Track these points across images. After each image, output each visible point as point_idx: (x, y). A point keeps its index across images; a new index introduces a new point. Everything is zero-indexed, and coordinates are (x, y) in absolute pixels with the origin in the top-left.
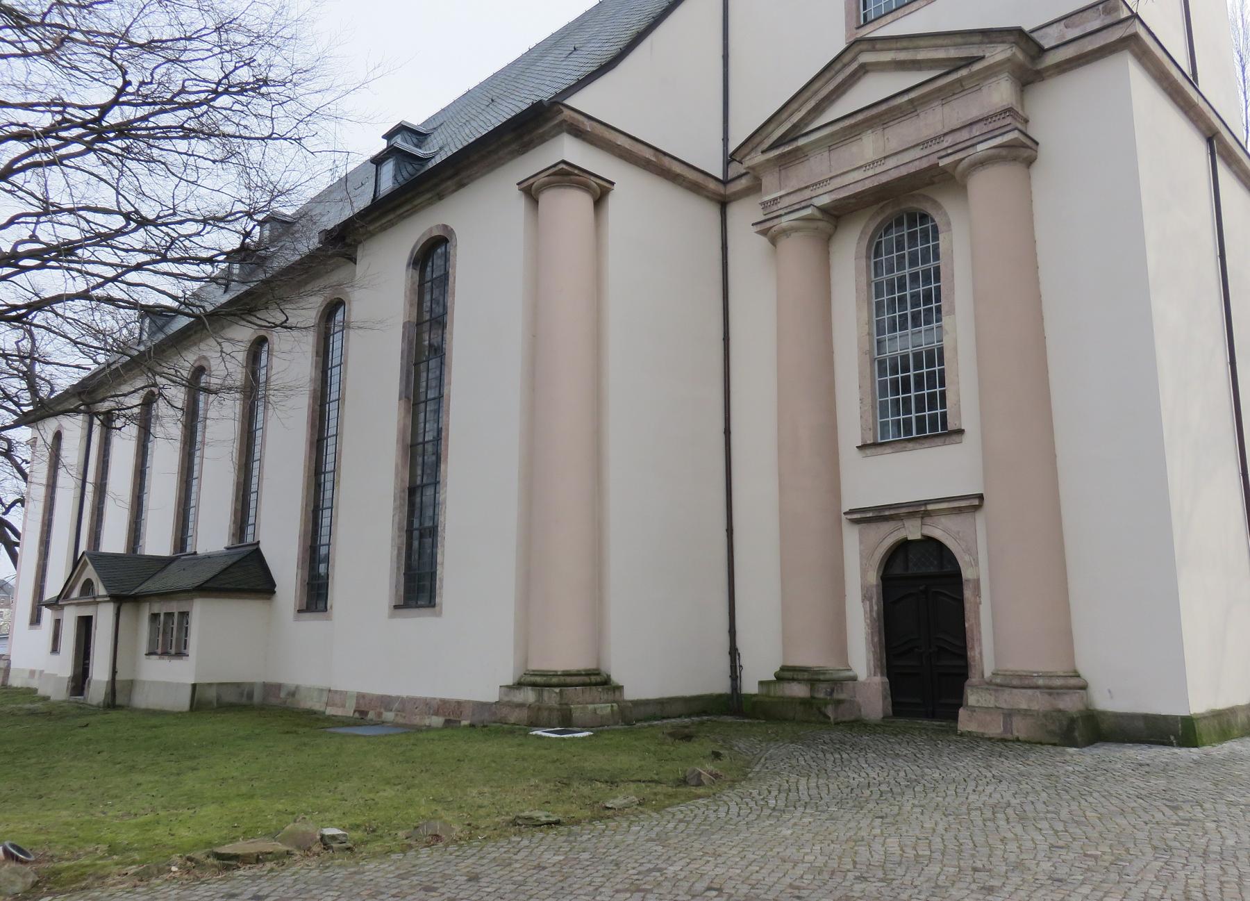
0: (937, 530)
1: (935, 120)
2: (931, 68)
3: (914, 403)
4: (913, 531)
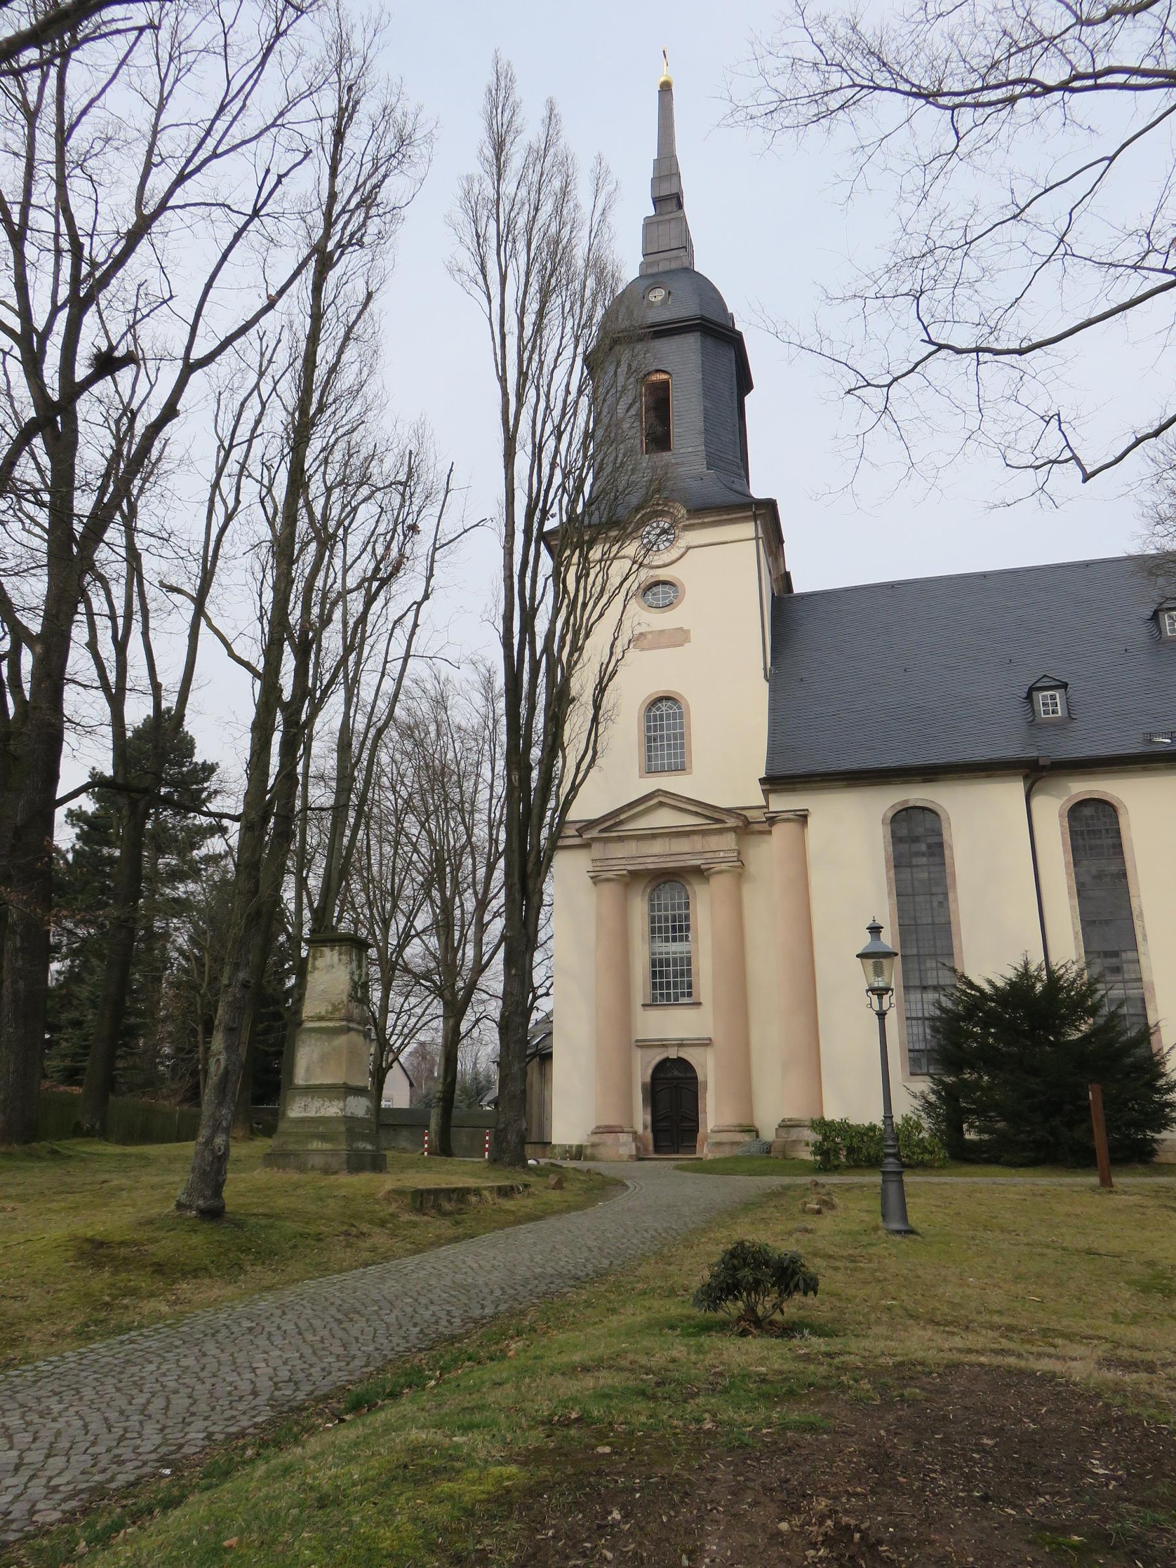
0: (686, 1054)
1: (697, 843)
3: (670, 983)
4: (673, 1054)
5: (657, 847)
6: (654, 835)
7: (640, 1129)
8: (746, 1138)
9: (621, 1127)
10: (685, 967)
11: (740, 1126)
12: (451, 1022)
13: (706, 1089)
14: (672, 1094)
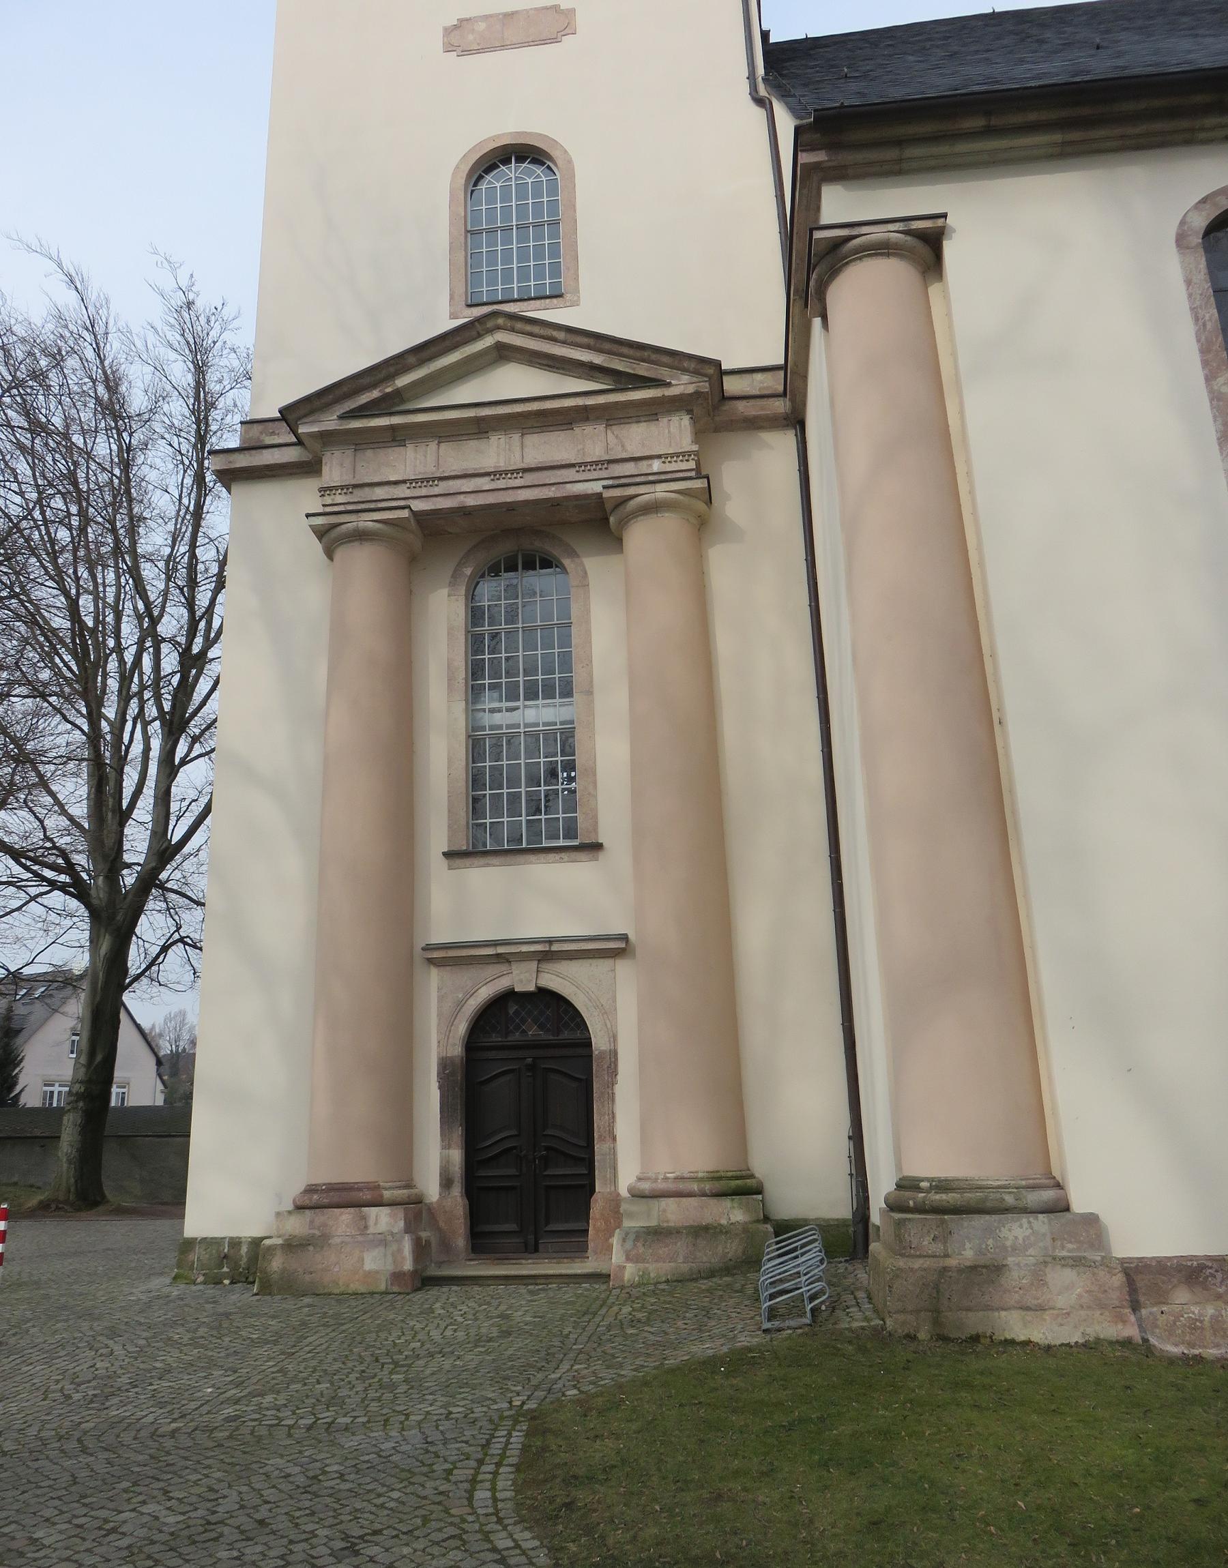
0: (559, 979)
1: (593, 442)
2: (590, 378)
3: (525, 804)
4: (523, 979)
5: (495, 452)
6: (481, 424)
7: (431, 1189)
8: (734, 1213)
9: (375, 1187)
10: (562, 758)
11: (715, 1177)
12: (105, 946)
13: (613, 1071)
14: (523, 1086)
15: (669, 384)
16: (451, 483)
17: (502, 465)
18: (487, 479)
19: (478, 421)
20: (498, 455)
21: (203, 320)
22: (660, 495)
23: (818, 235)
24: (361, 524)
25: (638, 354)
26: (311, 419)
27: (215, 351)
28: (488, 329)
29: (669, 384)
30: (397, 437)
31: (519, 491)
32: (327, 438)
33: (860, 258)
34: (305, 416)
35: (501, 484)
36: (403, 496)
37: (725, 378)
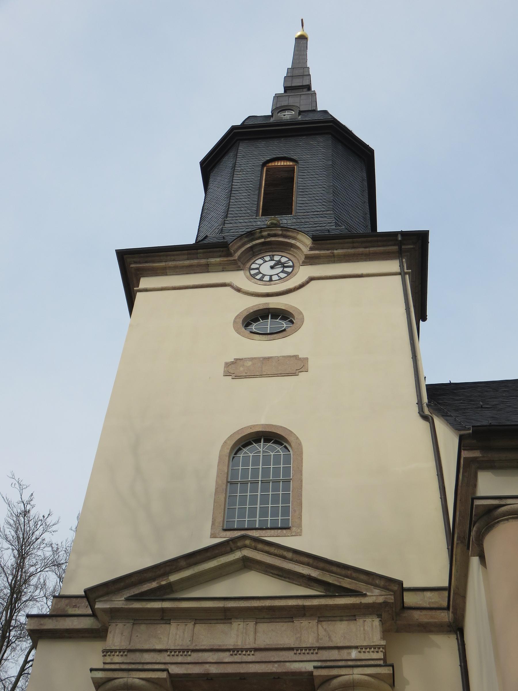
1: (308, 633)
2: (308, 586)
5: (235, 634)
6: (226, 613)
15: (365, 595)
16: (200, 654)
17: (240, 644)
18: (228, 654)
19: (225, 610)
20: (238, 636)
21: (32, 523)
22: (357, 677)
23: (477, 502)
24: (130, 681)
25: (344, 572)
26: (105, 598)
27: (35, 545)
28: (239, 547)
29: (365, 595)
30: (165, 617)
31: (251, 665)
32: (115, 614)
33: (507, 520)
34: (102, 596)
35: (237, 658)
36: (164, 661)
37: (405, 594)
